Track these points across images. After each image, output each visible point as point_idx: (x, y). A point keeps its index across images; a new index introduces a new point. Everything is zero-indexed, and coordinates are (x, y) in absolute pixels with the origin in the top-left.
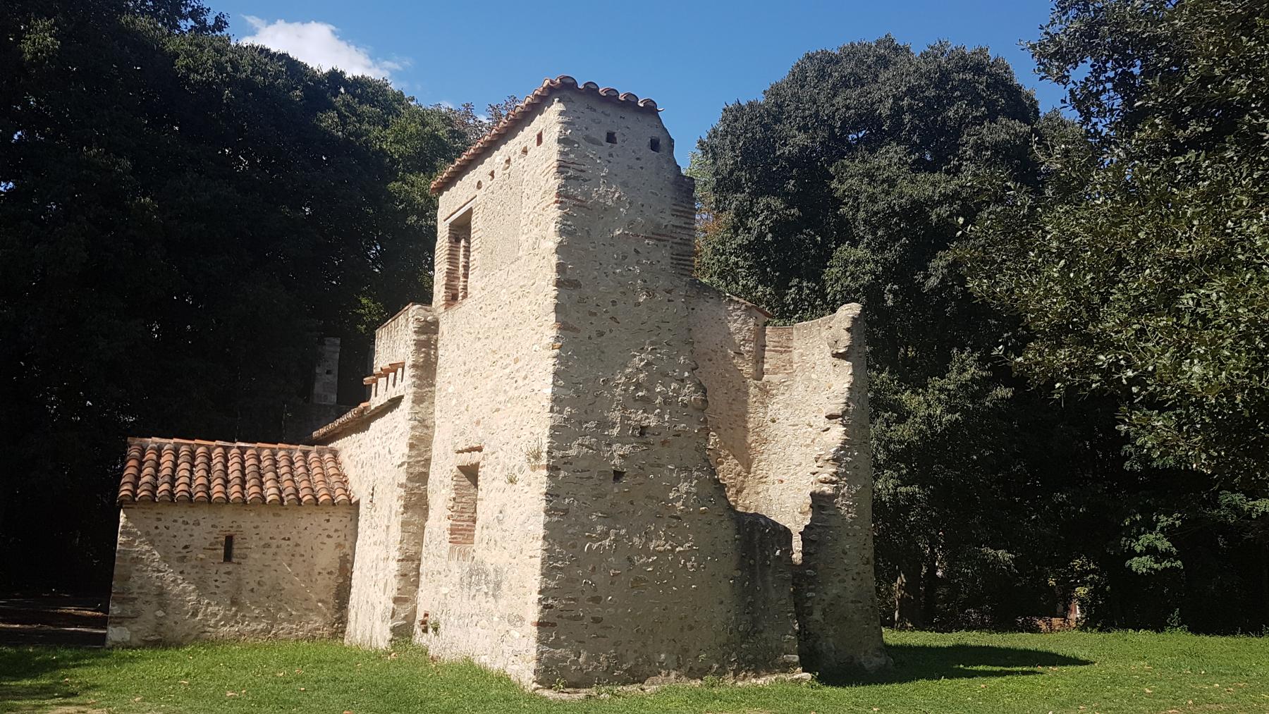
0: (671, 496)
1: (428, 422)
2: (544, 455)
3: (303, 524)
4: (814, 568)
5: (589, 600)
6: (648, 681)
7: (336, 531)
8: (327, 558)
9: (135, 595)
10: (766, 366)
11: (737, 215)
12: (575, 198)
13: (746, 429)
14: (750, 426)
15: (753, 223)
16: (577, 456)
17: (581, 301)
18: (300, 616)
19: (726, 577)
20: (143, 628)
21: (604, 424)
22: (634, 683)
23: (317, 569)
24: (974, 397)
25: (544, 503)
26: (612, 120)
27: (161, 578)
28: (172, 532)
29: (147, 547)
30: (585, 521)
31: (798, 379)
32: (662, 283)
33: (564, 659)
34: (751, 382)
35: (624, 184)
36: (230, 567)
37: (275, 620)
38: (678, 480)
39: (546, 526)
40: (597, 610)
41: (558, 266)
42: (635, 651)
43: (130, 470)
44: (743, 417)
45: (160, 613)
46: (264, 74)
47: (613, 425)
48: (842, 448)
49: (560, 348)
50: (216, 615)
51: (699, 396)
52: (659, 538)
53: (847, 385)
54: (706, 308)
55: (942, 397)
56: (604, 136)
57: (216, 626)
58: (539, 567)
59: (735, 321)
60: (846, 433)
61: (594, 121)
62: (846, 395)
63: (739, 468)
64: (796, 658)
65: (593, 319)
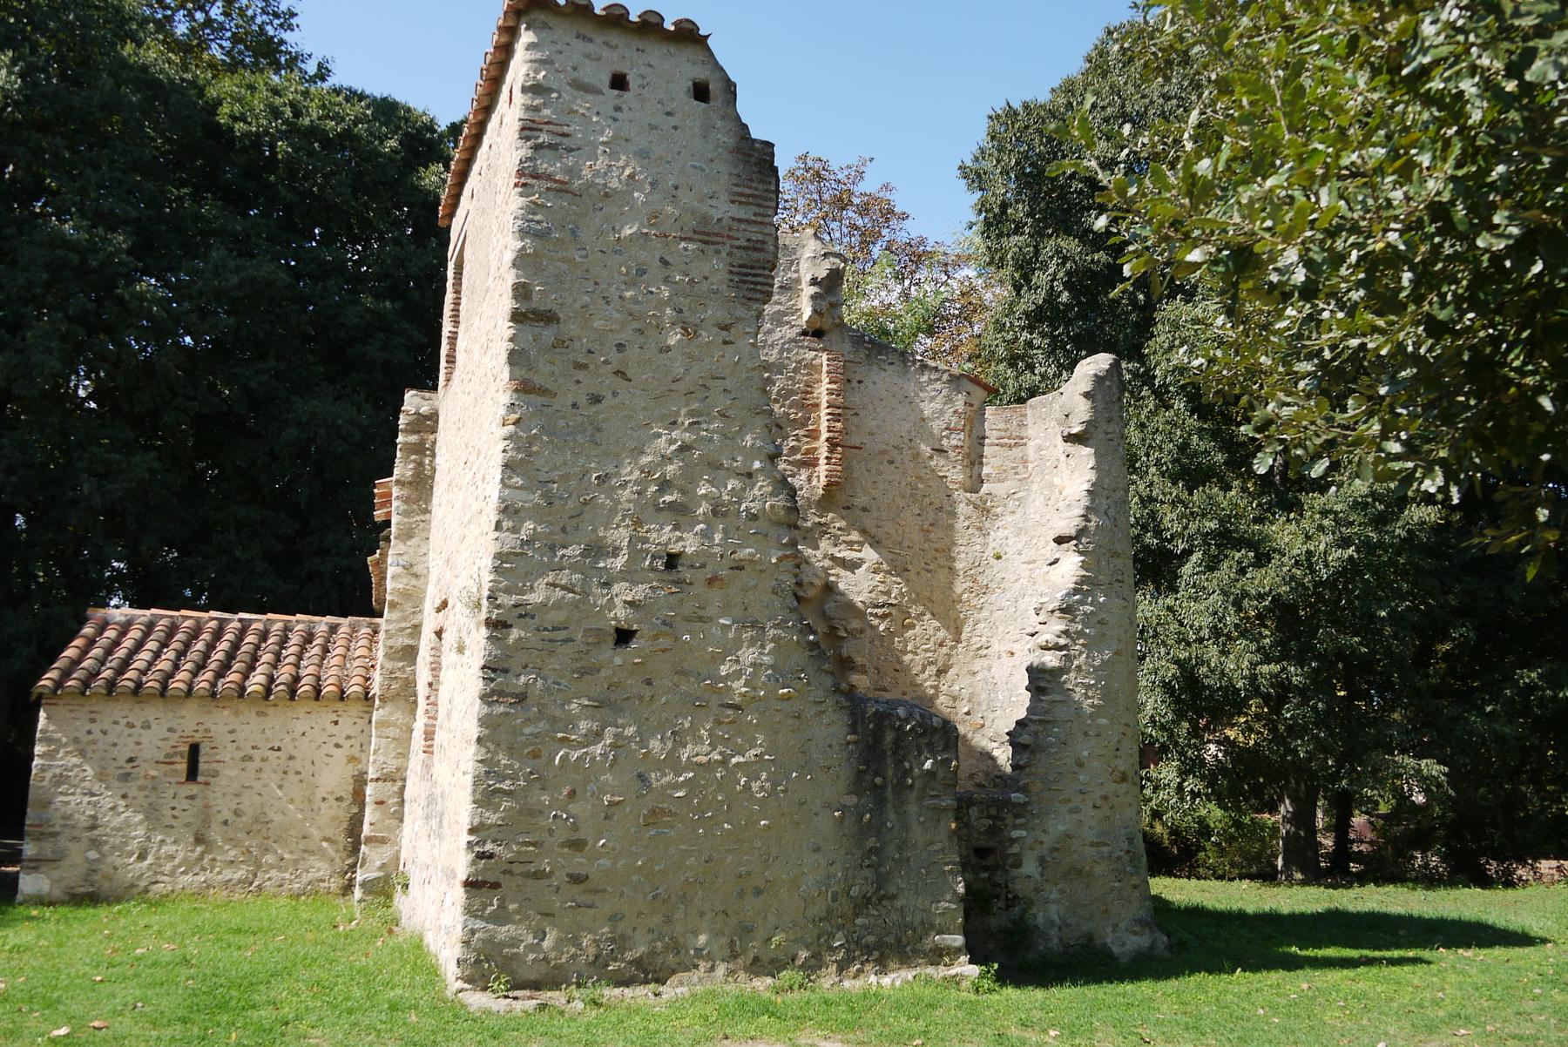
1: (418, 569)
2: (485, 602)
3: (300, 726)
4: (1024, 789)
5: (562, 845)
6: (674, 979)
7: (348, 737)
8: (334, 777)
9: (57, 829)
10: (986, 470)
11: (1019, 267)
12: (549, 177)
14: (959, 565)
15: (1040, 278)
17: (559, 344)
18: (296, 861)
20: (71, 872)
21: (597, 550)
22: (646, 982)
23: (321, 793)
24: (1380, 521)
25: (481, 683)
26: (621, 54)
27: (95, 804)
28: (111, 738)
29: (75, 760)
30: (558, 713)
31: (1035, 487)
32: (713, 312)
33: (515, 942)
35: (643, 155)
36: (193, 789)
37: (259, 865)
38: (738, 644)
39: (484, 721)
40: (578, 862)
42: (651, 931)
43: (70, 652)
45: (93, 855)
46: (339, 119)
47: (615, 552)
48: (1076, 591)
49: (517, 422)
50: (172, 857)
51: (780, 501)
52: (698, 740)
53: (1086, 486)
54: (882, 380)
55: (1326, 522)
57: (172, 874)
58: (469, 789)
59: (933, 399)
60: (1084, 566)
61: (587, 56)
62: (1085, 502)
63: (942, 634)
64: (958, 940)
65: (581, 375)
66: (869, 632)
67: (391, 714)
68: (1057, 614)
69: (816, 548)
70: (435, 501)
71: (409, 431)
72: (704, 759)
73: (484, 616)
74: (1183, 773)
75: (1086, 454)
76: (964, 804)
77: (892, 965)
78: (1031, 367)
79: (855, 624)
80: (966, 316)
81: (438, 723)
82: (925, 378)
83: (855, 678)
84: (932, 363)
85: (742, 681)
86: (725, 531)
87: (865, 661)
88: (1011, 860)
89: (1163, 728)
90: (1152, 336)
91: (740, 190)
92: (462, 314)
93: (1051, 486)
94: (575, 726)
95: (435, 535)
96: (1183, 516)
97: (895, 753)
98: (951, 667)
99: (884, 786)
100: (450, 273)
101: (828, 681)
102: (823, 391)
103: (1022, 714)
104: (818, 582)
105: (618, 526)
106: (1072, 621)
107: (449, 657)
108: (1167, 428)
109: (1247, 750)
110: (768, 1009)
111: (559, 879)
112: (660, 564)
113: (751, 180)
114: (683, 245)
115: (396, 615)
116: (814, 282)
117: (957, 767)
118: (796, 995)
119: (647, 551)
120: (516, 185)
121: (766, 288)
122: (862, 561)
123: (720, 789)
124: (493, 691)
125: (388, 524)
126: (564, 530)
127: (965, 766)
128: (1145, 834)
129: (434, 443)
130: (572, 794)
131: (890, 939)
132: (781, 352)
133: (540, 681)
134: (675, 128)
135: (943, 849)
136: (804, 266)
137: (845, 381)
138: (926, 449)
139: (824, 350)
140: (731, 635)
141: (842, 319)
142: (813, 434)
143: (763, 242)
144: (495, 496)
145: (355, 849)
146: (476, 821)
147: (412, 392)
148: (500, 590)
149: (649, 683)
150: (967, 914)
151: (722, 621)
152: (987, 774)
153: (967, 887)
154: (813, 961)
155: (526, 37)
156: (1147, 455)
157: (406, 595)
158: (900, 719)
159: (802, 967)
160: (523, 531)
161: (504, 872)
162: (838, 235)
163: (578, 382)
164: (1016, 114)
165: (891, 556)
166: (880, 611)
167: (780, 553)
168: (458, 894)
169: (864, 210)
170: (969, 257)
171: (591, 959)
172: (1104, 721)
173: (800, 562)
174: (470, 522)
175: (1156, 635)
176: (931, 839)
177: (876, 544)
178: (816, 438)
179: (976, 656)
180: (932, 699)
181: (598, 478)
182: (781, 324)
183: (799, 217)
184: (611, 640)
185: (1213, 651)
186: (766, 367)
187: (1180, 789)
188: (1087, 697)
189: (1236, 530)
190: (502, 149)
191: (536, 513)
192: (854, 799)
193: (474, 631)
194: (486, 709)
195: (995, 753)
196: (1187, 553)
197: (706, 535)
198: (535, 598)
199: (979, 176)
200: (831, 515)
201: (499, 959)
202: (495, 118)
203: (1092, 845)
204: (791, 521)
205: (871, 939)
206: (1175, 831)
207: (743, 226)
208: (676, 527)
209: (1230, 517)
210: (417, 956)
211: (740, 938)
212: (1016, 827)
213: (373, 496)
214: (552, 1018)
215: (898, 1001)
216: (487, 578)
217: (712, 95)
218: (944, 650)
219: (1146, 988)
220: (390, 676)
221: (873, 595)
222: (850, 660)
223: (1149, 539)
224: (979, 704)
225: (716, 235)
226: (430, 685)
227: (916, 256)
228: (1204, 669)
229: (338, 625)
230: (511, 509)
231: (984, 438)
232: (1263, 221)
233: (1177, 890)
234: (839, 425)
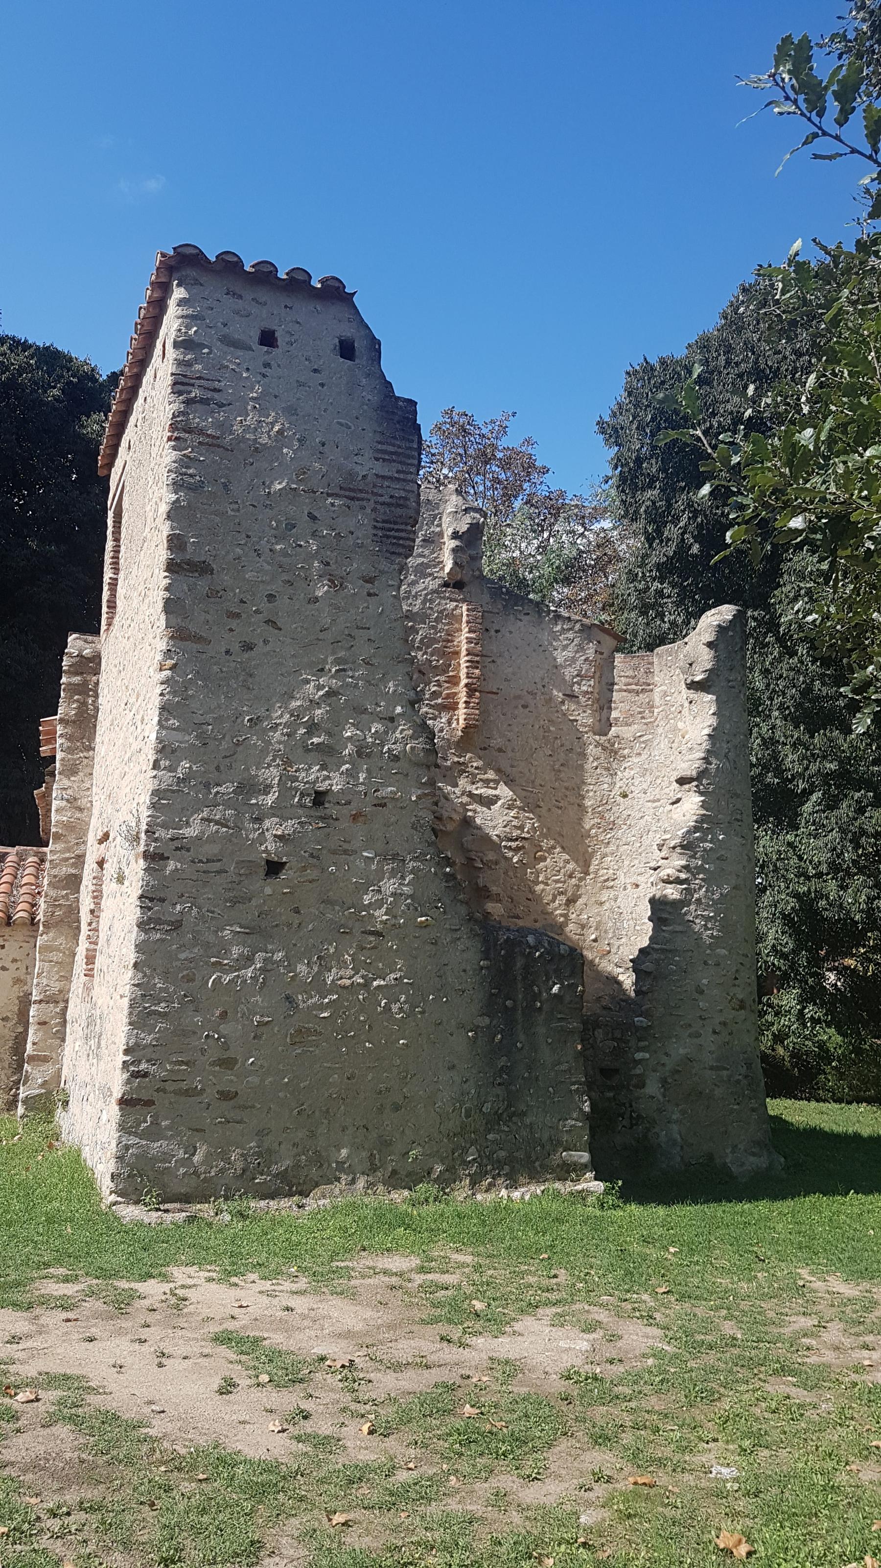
0: (367, 899)
2: (143, 836)
4: (647, 1014)
5: (213, 1064)
6: (317, 1191)
7: (14, 961)
10: (614, 714)
12: (201, 432)
13: (582, 808)
14: (588, 803)
15: (672, 531)
16: (198, 838)
17: (213, 594)
19: (461, 1026)
21: (249, 787)
22: (291, 1195)
26: (270, 311)
30: (211, 939)
31: (660, 730)
32: (358, 566)
33: (166, 1157)
34: (589, 738)
35: (291, 411)
39: (140, 948)
40: (228, 1080)
41: (171, 539)
44: (577, 791)
48: (696, 829)
49: (173, 668)
51: (419, 744)
52: (343, 965)
53: (707, 731)
54: (517, 629)
56: (255, 335)
58: (126, 1012)
59: (565, 647)
61: (237, 313)
62: (706, 745)
63: (571, 866)
65: (234, 623)
66: (503, 863)
67: (54, 939)
68: (678, 850)
69: (456, 785)
70: (98, 739)
71: (73, 672)
72: (348, 982)
73: (142, 848)
74: (803, 1000)
75: (707, 701)
76: (589, 1025)
77: (522, 1180)
78: (661, 616)
79: (491, 856)
80: (601, 567)
81: (98, 948)
82: (559, 628)
83: (490, 906)
84: (565, 613)
85: (384, 910)
86: (368, 771)
87: (500, 891)
88: (634, 1081)
89: (784, 956)
90: (779, 586)
91: (384, 447)
92: (122, 561)
93: (675, 729)
94: (228, 951)
95: (98, 771)
96: (805, 757)
97: (524, 978)
98: (580, 896)
99: (514, 1009)
100: (110, 522)
101: (463, 910)
102: (463, 638)
103: (645, 943)
104: (456, 817)
105: (269, 766)
106: (693, 857)
107: (110, 887)
108: (779, 677)
109: (864, 978)
110: (405, 1221)
111: (210, 1095)
112: (308, 801)
113: (394, 438)
114: (330, 500)
115: (59, 846)
116: (455, 535)
117: (583, 992)
118: (431, 1208)
119: (296, 789)
120: (169, 439)
121: (408, 543)
122: (497, 798)
123: (362, 1010)
124: (150, 919)
125: (53, 759)
126: (218, 768)
127: (591, 989)
128: (764, 1057)
129: (97, 684)
130: (224, 1015)
131: (520, 1155)
132: (424, 602)
133: (195, 910)
134: (322, 385)
135: (569, 1070)
136: (446, 520)
137: (484, 630)
138: (558, 695)
139: (464, 601)
140: (373, 867)
141: (481, 572)
142: (454, 681)
143: (406, 499)
144: (153, 736)
145: (20, 1067)
146: (132, 1042)
147: (74, 636)
148: (158, 825)
149: (297, 911)
150: (592, 1135)
151: (365, 854)
152: (613, 997)
153: (592, 1106)
154: (447, 1175)
155: (178, 293)
156: (772, 699)
157: (70, 827)
158: (530, 947)
159: (435, 1181)
160: (179, 769)
161: (158, 1090)
162: (481, 488)
163: (231, 630)
164: (652, 369)
165: (524, 794)
166: (513, 844)
167: (419, 792)
168: (113, 1112)
169: (506, 464)
170: (605, 510)
171: (239, 1172)
172: (724, 952)
173: (437, 799)
174: (130, 759)
175: (776, 870)
176: (558, 1058)
177: (510, 782)
178: (456, 684)
179: (603, 888)
180: (562, 927)
181: (250, 720)
182: (424, 576)
183: (445, 471)
184: (262, 872)
185: (832, 886)
186: (409, 616)
187: (801, 1013)
188: (706, 928)
189: (856, 771)
190: (155, 403)
191: (191, 753)
192: (487, 1020)
193: (133, 861)
194: (143, 936)
195: (621, 978)
196: (807, 794)
197: (351, 774)
198: (192, 831)
199: (616, 430)
200: (469, 755)
201: (150, 1173)
202: (150, 372)
203: (712, 1068)
204: (431, 762)
205: (502, 1154)
206: (795, 1055)
207: (386, 483)
208: (323, 767)
209: (849, 758)
210: (75, 1168)
211: (380, 1151)
212: (639, 1049)
213: (39, 733)
214: (200, 1229)
215: (525, 1215)
216: (145, 814)
217: (357, 353)
218: (574, 881)
219: (763, 1207)
220: (53, 904)
221: (507, 829)
222: (486, 888)
223: (770, 778)
224: (606, 932)
225: (361, 491)
226: (92, 912)
227: (554, 508)
228: (823, 903)
229: (8, 853)
230: (168, 750)
231: (613, 684)
232: (860, 491)
233: (799, 1112)
234: (477, 671)
